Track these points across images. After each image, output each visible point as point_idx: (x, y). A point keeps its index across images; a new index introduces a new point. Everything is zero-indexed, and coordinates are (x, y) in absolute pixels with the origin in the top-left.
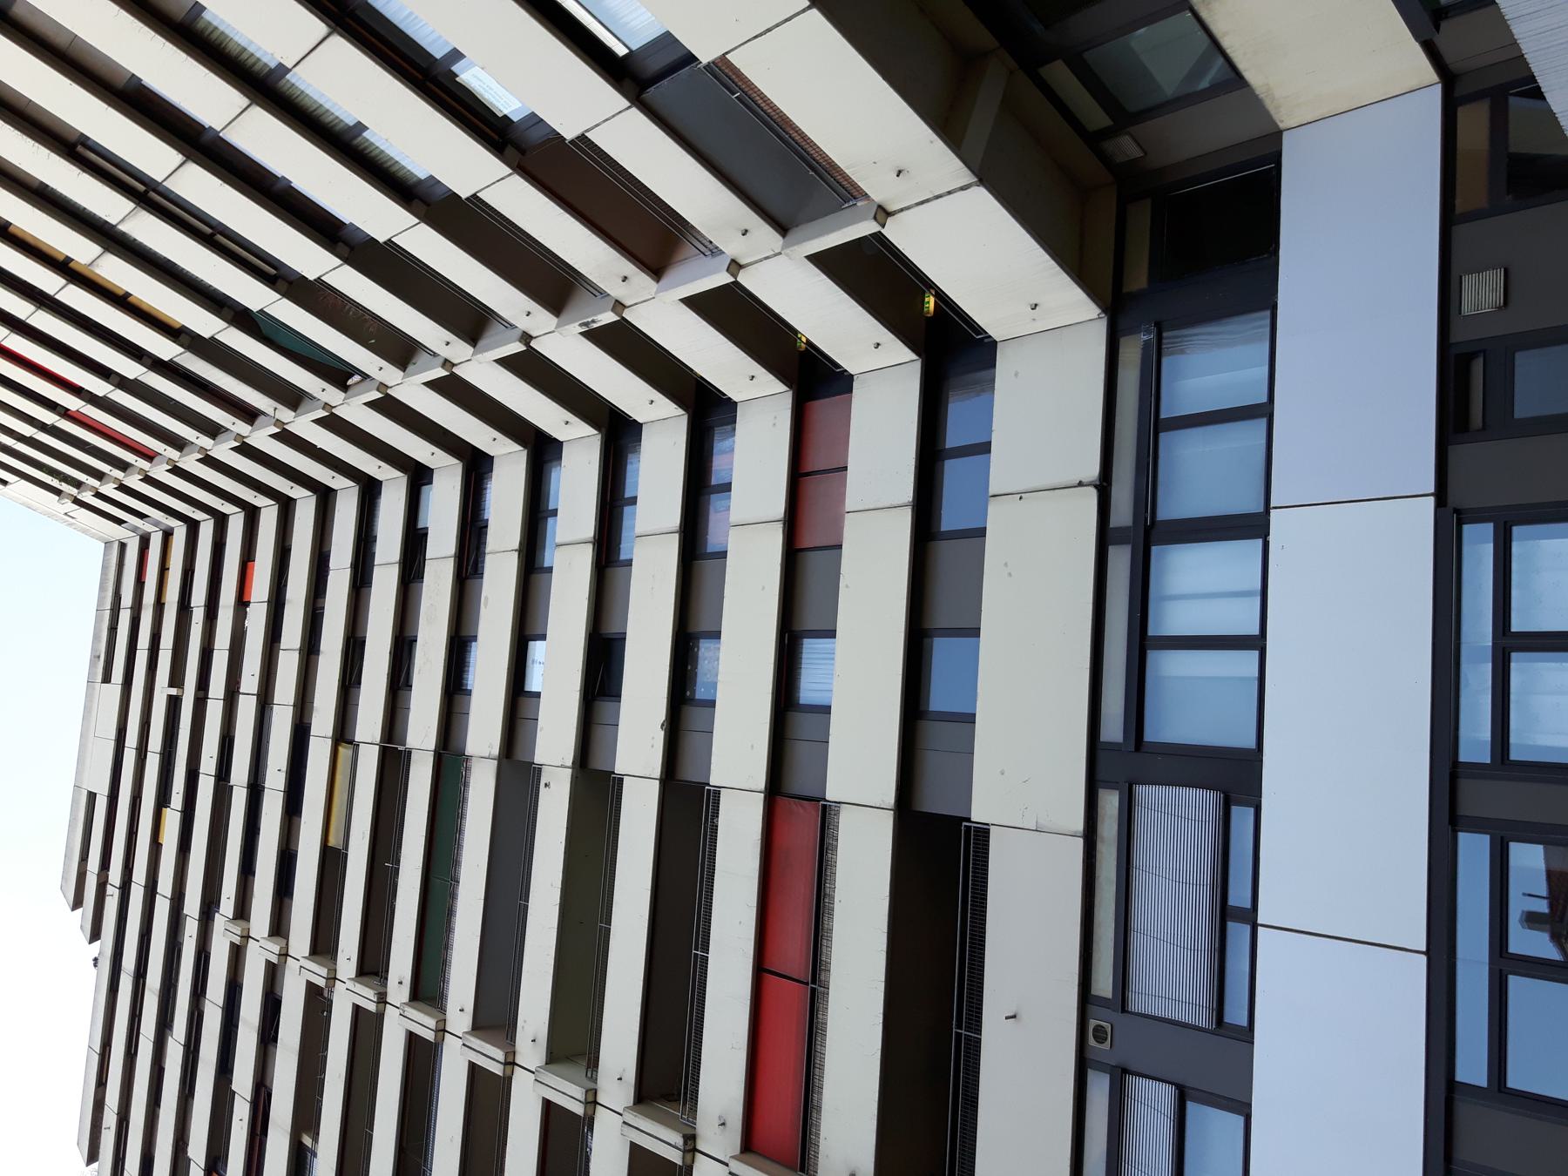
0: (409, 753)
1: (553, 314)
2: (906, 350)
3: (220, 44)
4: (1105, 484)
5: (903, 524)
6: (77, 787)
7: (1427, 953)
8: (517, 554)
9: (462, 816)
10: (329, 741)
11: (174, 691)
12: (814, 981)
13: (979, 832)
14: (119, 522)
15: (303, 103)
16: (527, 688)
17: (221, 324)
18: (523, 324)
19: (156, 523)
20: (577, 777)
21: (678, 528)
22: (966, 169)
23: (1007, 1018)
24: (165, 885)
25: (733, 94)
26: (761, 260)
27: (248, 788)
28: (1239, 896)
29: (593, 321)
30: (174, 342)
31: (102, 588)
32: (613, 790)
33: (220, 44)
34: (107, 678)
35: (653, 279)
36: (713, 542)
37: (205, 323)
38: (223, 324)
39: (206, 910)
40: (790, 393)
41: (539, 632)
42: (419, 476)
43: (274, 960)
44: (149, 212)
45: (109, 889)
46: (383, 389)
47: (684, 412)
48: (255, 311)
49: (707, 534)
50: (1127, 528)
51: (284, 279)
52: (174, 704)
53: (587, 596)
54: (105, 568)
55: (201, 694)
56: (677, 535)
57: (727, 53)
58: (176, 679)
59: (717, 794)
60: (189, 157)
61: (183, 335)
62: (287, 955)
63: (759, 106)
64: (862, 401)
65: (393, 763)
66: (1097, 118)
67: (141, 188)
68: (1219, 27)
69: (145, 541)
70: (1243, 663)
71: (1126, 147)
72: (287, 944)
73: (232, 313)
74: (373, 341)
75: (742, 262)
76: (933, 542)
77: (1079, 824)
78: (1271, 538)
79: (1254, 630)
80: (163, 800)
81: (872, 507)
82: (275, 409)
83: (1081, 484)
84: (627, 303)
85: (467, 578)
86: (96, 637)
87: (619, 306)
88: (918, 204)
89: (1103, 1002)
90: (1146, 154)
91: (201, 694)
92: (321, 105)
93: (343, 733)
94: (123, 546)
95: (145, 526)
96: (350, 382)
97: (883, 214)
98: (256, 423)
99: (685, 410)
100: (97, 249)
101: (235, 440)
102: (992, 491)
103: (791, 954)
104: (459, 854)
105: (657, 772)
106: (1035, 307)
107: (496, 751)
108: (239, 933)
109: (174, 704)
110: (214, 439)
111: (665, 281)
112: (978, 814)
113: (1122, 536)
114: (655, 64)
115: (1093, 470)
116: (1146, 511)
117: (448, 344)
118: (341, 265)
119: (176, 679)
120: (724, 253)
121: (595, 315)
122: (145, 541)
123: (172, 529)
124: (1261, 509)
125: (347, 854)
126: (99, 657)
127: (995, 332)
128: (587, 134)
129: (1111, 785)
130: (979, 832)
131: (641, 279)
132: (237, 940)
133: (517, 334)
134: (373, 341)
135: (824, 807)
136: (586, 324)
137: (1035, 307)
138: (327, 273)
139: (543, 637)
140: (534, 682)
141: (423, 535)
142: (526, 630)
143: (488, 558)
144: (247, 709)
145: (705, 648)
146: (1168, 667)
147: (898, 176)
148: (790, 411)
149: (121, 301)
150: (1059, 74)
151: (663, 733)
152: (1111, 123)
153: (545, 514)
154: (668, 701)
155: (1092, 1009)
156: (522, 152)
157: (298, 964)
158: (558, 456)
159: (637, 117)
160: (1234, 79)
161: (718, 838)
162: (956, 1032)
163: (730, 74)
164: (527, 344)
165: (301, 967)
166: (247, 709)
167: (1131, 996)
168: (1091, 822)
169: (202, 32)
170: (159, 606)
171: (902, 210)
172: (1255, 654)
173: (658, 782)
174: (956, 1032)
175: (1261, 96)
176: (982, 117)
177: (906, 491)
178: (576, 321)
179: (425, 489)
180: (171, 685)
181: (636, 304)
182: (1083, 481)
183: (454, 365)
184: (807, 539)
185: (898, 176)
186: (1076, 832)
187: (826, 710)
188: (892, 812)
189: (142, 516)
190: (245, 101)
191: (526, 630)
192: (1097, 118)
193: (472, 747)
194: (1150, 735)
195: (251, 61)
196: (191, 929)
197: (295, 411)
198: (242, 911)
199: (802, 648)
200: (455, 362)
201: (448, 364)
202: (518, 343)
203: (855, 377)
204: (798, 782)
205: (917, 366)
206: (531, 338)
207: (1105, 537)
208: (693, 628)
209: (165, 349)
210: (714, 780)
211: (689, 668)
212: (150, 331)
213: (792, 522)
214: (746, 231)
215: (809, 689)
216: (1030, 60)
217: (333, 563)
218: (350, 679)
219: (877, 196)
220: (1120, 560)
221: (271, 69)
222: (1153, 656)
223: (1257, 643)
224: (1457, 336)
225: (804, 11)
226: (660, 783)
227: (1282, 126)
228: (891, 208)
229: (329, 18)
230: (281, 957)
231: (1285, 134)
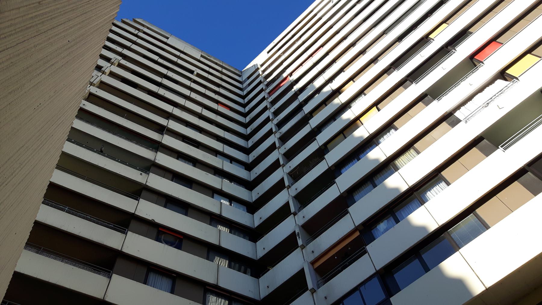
0: (162, 134)
1: (302, 225)
11: (195, 73)
14: (249, 78)
17: (313, 126)
27: (161, 83)
29: (299, 237)
37: (314, 122)
42: (249, 167)
43: (103, 69)
52: (192, 72)
53: (203, 207)
56: (218, 244)
58: (198, 75)
74: (298, 173)
84: (304, 250)
87: (303, 247)
94: (240, 76)
95: (245, 85)
107: (157, 161)
108: (114, 62)
109: (192, 72)
119: (198, 75)
121: (302, 239)
123: (243, 91)
132: (112, 61)
134: (298, 173)
138: (326, 161)
144: (187, 92)
151: (151, 219)
157: (99, 76)
158: (248, 211)
162: (7, 302)
165: (98, 76)
166: (187, 92)
174: (7, 302)
178: (300, 231)
181: (303, 253)
183: (288, 189)
193: (159, 154)
196: (119, 49)
198: (120, 66)
200: (289, 190)
202: (294, 211)
230: (103, 72)
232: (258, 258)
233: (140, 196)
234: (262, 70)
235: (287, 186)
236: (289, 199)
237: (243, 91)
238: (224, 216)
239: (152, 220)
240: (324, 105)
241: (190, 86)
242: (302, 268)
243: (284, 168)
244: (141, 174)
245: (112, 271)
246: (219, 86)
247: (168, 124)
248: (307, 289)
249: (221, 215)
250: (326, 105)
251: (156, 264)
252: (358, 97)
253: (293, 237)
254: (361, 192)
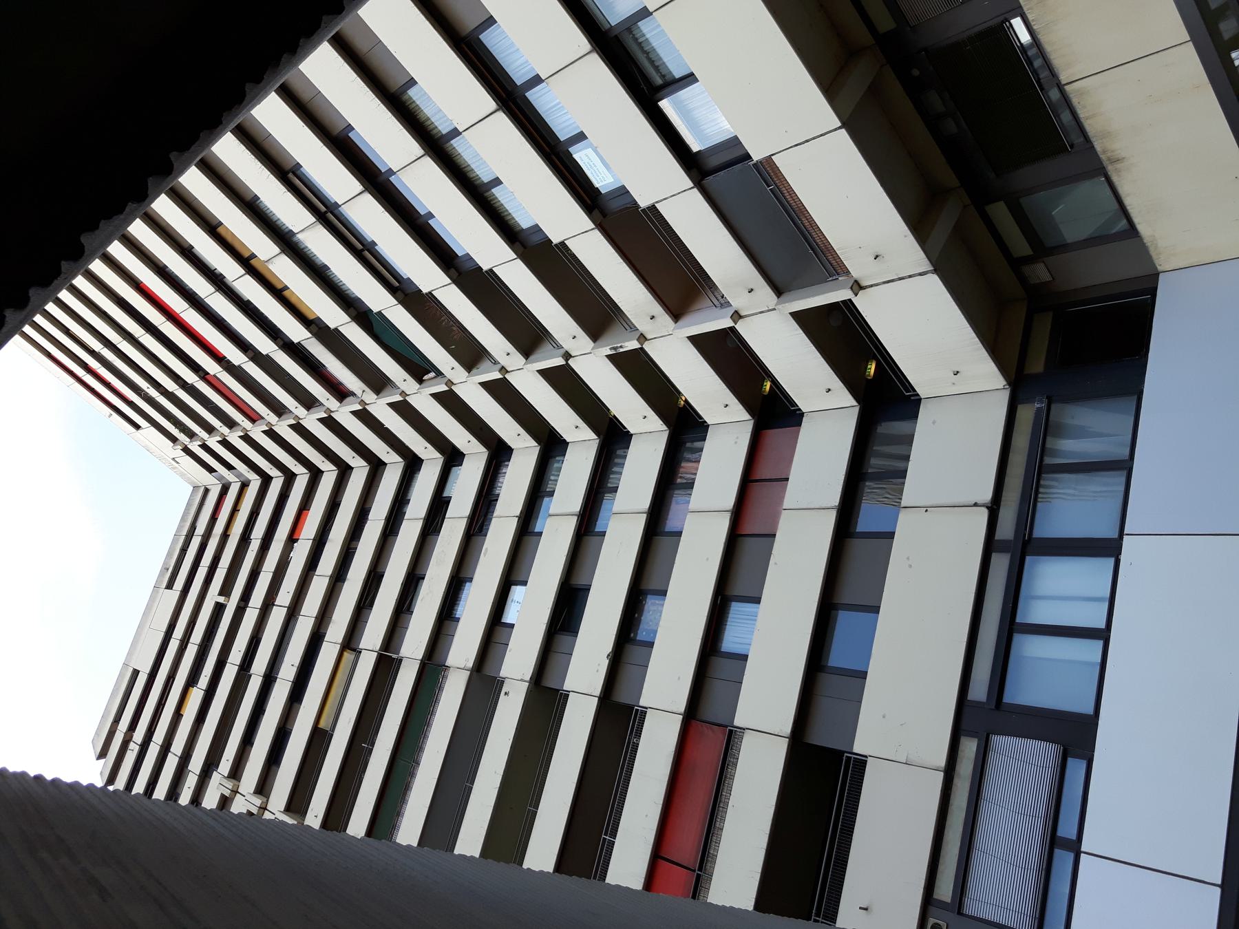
0: (400, 661)
2: (850, 397)
3: (415, 112)
4: (995, 507)
5: (828, 522)
6: (126, 665)
7: (1222, 886)
8: (517, 519)
9: (432, 713)
10: (338, 647)
11: (221, 599)
12: (700, 869)
13: (857, 762)
14: (211, 470)
15: (459, 161)
16: (504, 620)
17: (346, 318)
18: (568, 345)
19: (239, 475)
20: (531, 691)
21: (647, 510)
22: (926, 259)
23: (860, 908)
24: (178, 746)
25: (769, 186)
26: (756, 314)
28: (1067, 829)
29: (621, 347)
30: (306, 329)
31: (183, 519)
32: (559, 703)
33: (415, 112)
34: (170, 586)
35: (673, 320)
36: (671, 524)
38: (347, 319)
39: (206, 769)
40: (752, 422)
41: (522, 579)
42: (453, 457)
44: (323, 226)
45: (132, 745)
46: (449, 384)
47: (666, 429)
48: (375, 311)
49: (667, 519)
50: (1008, 541)
51: (403, 291)
52: (219, 609)
54: (189, 505)
55: (242, 604)
56: (645, 515)
57: (773, 155)
58: (226, 590)
59: (643, 714)
60: (367, 189)
61: (313, 325)
62: (265, 809)
63: (785, 197)
64: (807, 431)
65: (386, 667)
66: (1021, 247)
67: (323, 209)
68: (1124, 188)
69: (225, 489)
70: (1090, 650)
71: (1040, 272)
72: (268, 801)
73: (356, 313)
74: (453, 347)
75: (743, 313)
77: (942, 761)
78: (1122, 557)
79: (1101, 624)
80: (192, 680)
82: (364, 391)
83: (976, 505)
84: (649, 337)
85: (473, 535)
86: (169, 555)
87: (642, 338)
88: (884, 283)
89: (942, 905)
90: (1053, 279)
91: (242, 604)
92: (469, 165)
93: (350, 643)
94: (207, 491)
96: (426, 377)
97: (857, 287)
98: (344, 401)
99: (668, 427)
100: (275, 249)
101: (325, 412)
103: (685, 846)
104: (424, 743)
105: (598, 692)
106: (956, 373)
107: (470, 664)
109: (219, 609)
110: (308, 411)
111: (680, 323)
112: (860, 746)
113: (1004, 547)
114: (714, 162)
115: (987, 495)
117: (508, 354)
118: (450, 284)
119: (226, 590)
120: (731, 305)
122: (225, 489)
124: (1116, 536)
125: (332, 735)
126: (168, 569)
127: (922, 391)
128: (656, 205)
129: (971, 734)
130: (857, 762)
131: (664, 319)
132: (227, 793)
133: (562, 351)
134: (453, 347)
135: (731, 731)
136: (615, 349)
137: (956, 373)
138: (437, 289)
139: (525, 583)
140: (510, 616)
141: (447, 501)
142: (513, 575)
143: (494, 520)
145: (650, 603)
146: (1030, 648)
147: (875, 259)
148: (750, 434)
149: (279, 293)
150: (1000, 212)
151: (608, 661)
152: (1032, 253)
153: (543, 494)
154: (616, 638)
155: (932, 910)
156: (604, 215)
159: (696, 195)
160: (1132, 231)
161: (636, 759)
163: (770, 172)
164: (567, 360)
167: (967, 901)
168: (951, 762)
169: (405, 103)
170: (225, 536)
171: (872, 286)
172: (1100, 643)
173: (597, 699)
175: (1148, 244)
176: (942, 231)
177: (834, 498)
179: (454, 469)
180: (221, 594)
181: (655, 338)
183: (507, 372)
184: (748, 527)
185: (875, 259)
186: (938, 767)
187: (744, 658)
188: (787, 740)
189: (229, 467)
190: (421, 152)
191: (513, 575)
192: (1021, 247)
194: (1008, 698)
195: (432, 127)
197: (377, 395)
198: (236, 772)
199: (730, 609)
200: (509, 369)
201: (503, 370)
203: (805, 414)
204: (711, 710)
205: (857, 410)
206: (571, 356)
207: (990, 545)
208: (644, 586)
209: (296, 332)
210: (643, 702)
211: (636, 615)
213: (739, 513)
214: (752, 290)
215: (731, 641)
216: (980, 197)
217: (372, 515)
218: (365, 603)
219: (855, 273)
220: (1001, 563)
221: (442, 135)
222: (1018, 639)
223: (1103, 635)
225: (836, 130)
226: (599, 700)
227: (1160, 269)
228: (864, 284)
231: (1161, 275)
232: (665, 427)
233: (558, 690)
234: (188, 440)
235: (502, 375)
236: (533, 371)
239: (610, 657)
240: (286, 293)
241: (260, 609)
242: (687, 339)
243: (455, 382)
245: (636, 708)
247: (371, 649)
248: (732, 329)
249: (578, 513)
250: (286, 288)
251: (702, 639)
252: (269, 218)
253: (622, 362)
254: (508, 208)
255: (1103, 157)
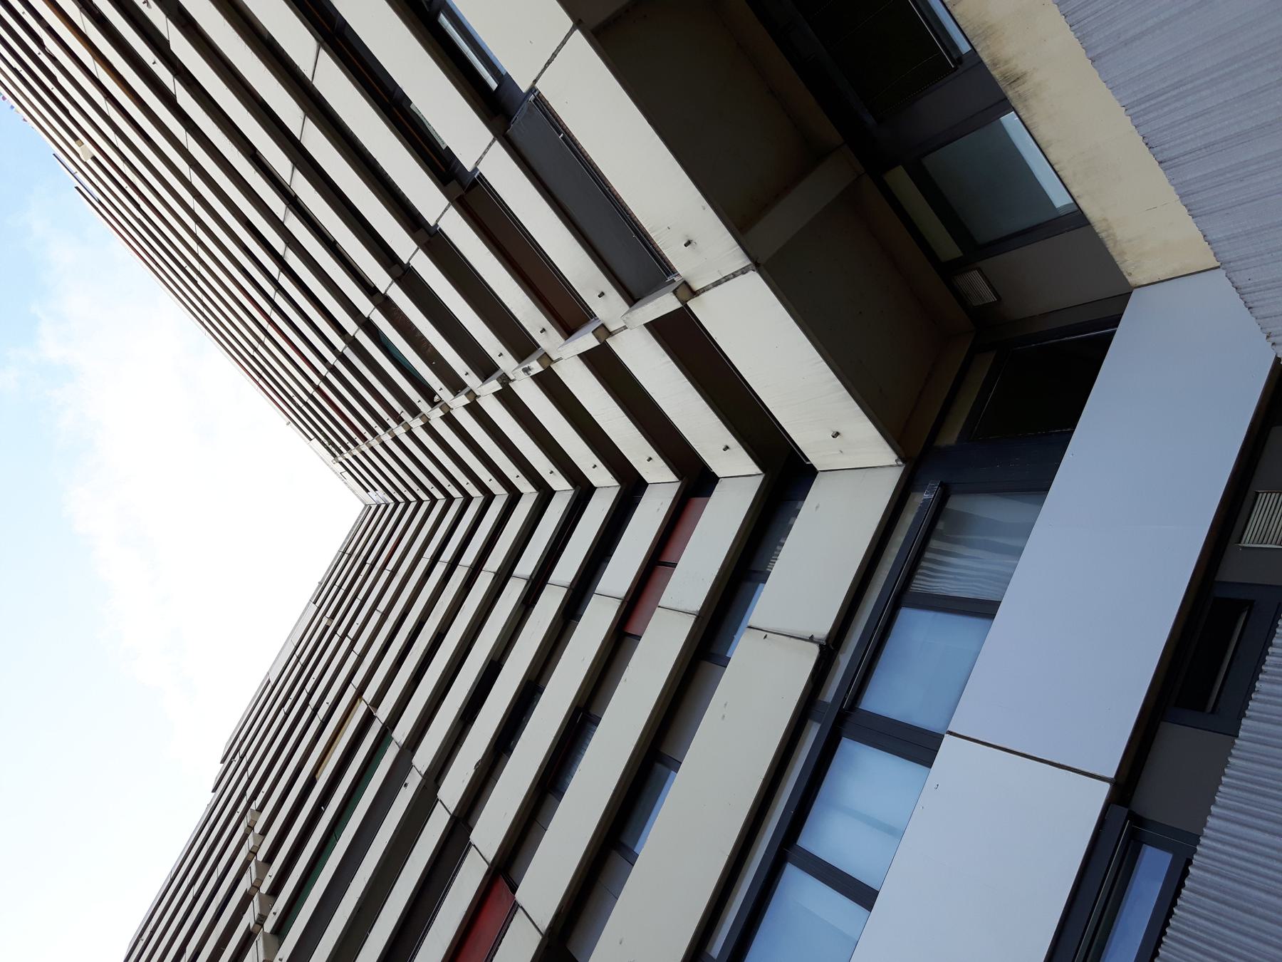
22: (738, 247)
30: (340, 336)
52: (327, 628)
66: (949, 249)
76: (706, 662)
81: (674, 607)
102: (660, 604)
106: (836, 434)
109: (327, 628)
116: (848, 692)
122: (379, 507)
150: (899, 178)
175: (1103, 235)
182: (815, 636)
185: (686, 245)
192: (949, 249)
212: (325, 323)
224: (1231, 572)
227: (1131, 280)
229: (320, 33)
230: (251, 854)
237: (389, 504)
238: (534, 571)
244: (406, 785)
246: (364, 563)
249: (528, 578)
255: (995, 73)
